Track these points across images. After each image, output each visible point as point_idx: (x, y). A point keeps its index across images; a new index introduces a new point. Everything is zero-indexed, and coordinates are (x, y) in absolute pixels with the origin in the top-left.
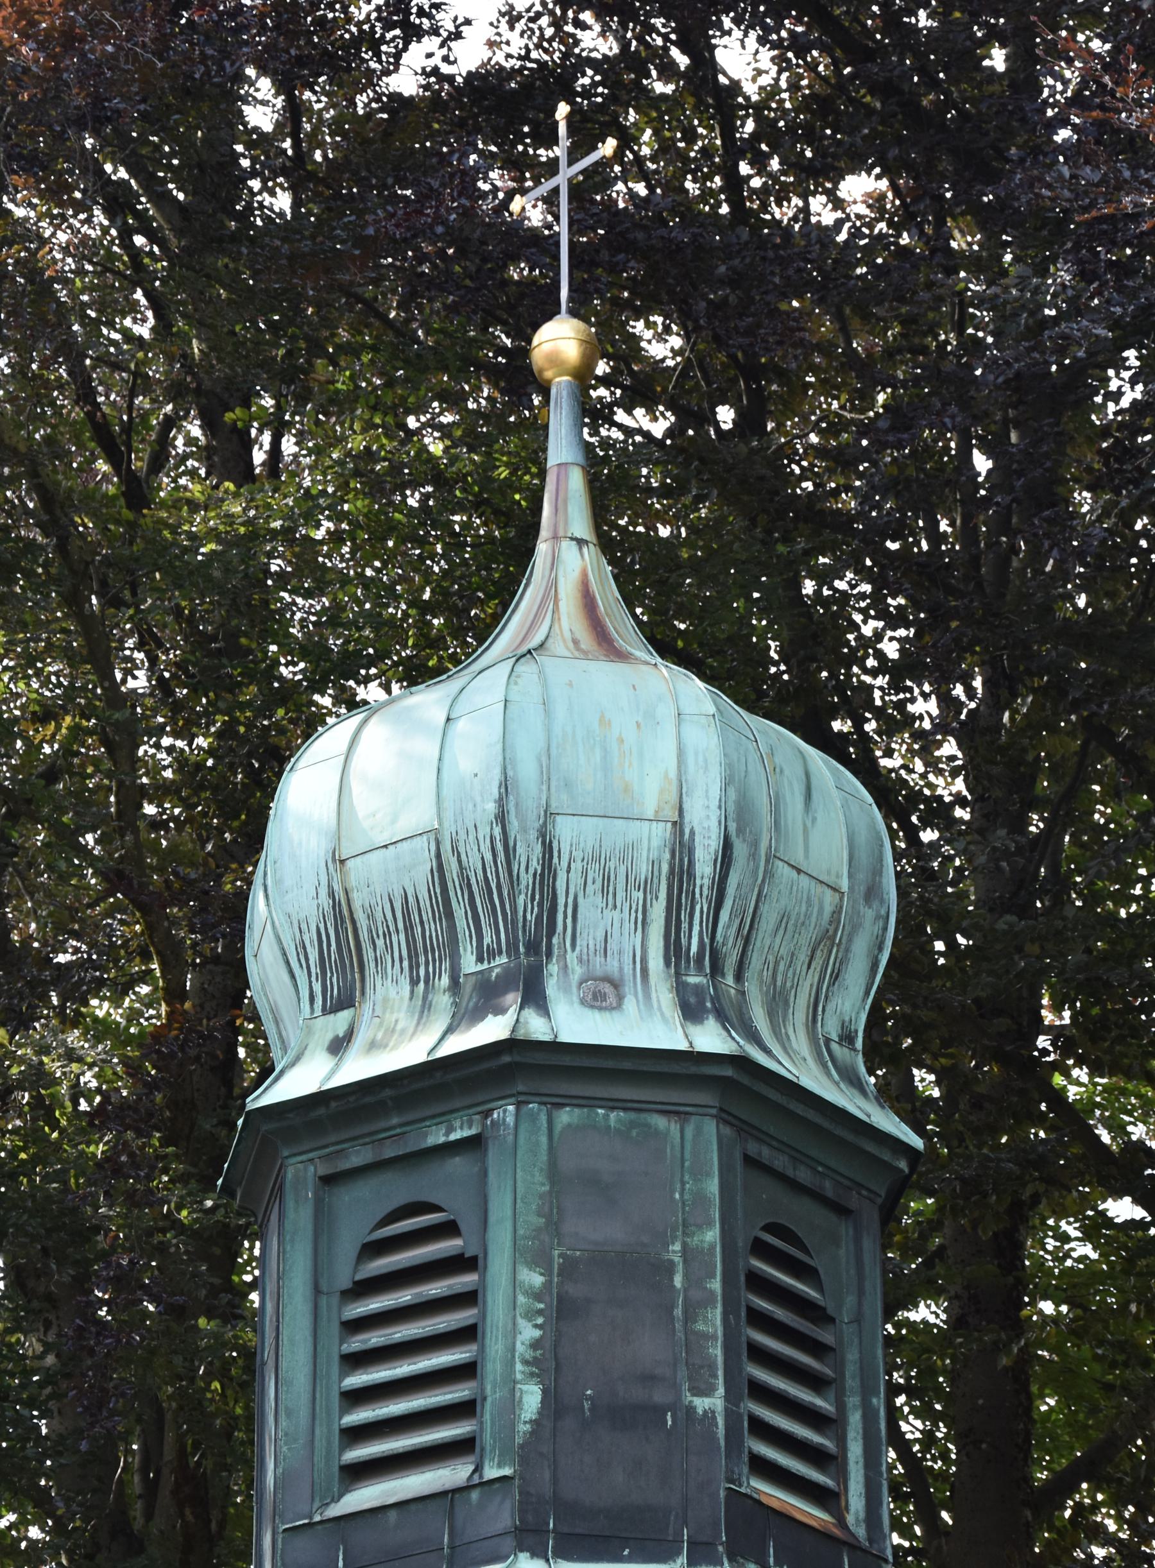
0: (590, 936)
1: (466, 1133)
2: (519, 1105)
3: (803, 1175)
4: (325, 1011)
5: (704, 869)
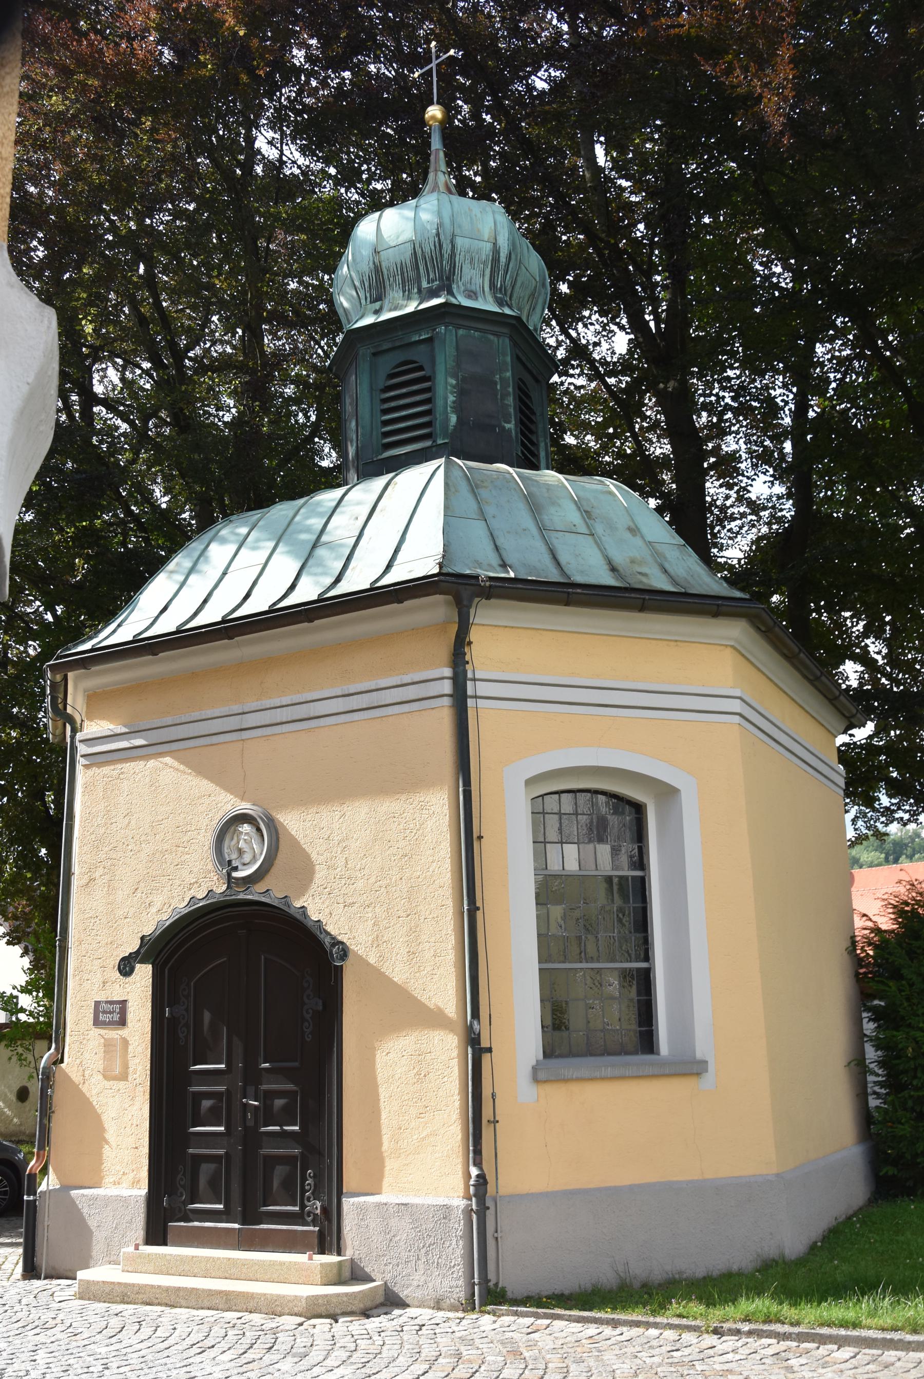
0: (466, 278)
1: (427, 336)
2: (446, 327)
3: (529, 365)
4: (371, 302)
5: (503, 260)
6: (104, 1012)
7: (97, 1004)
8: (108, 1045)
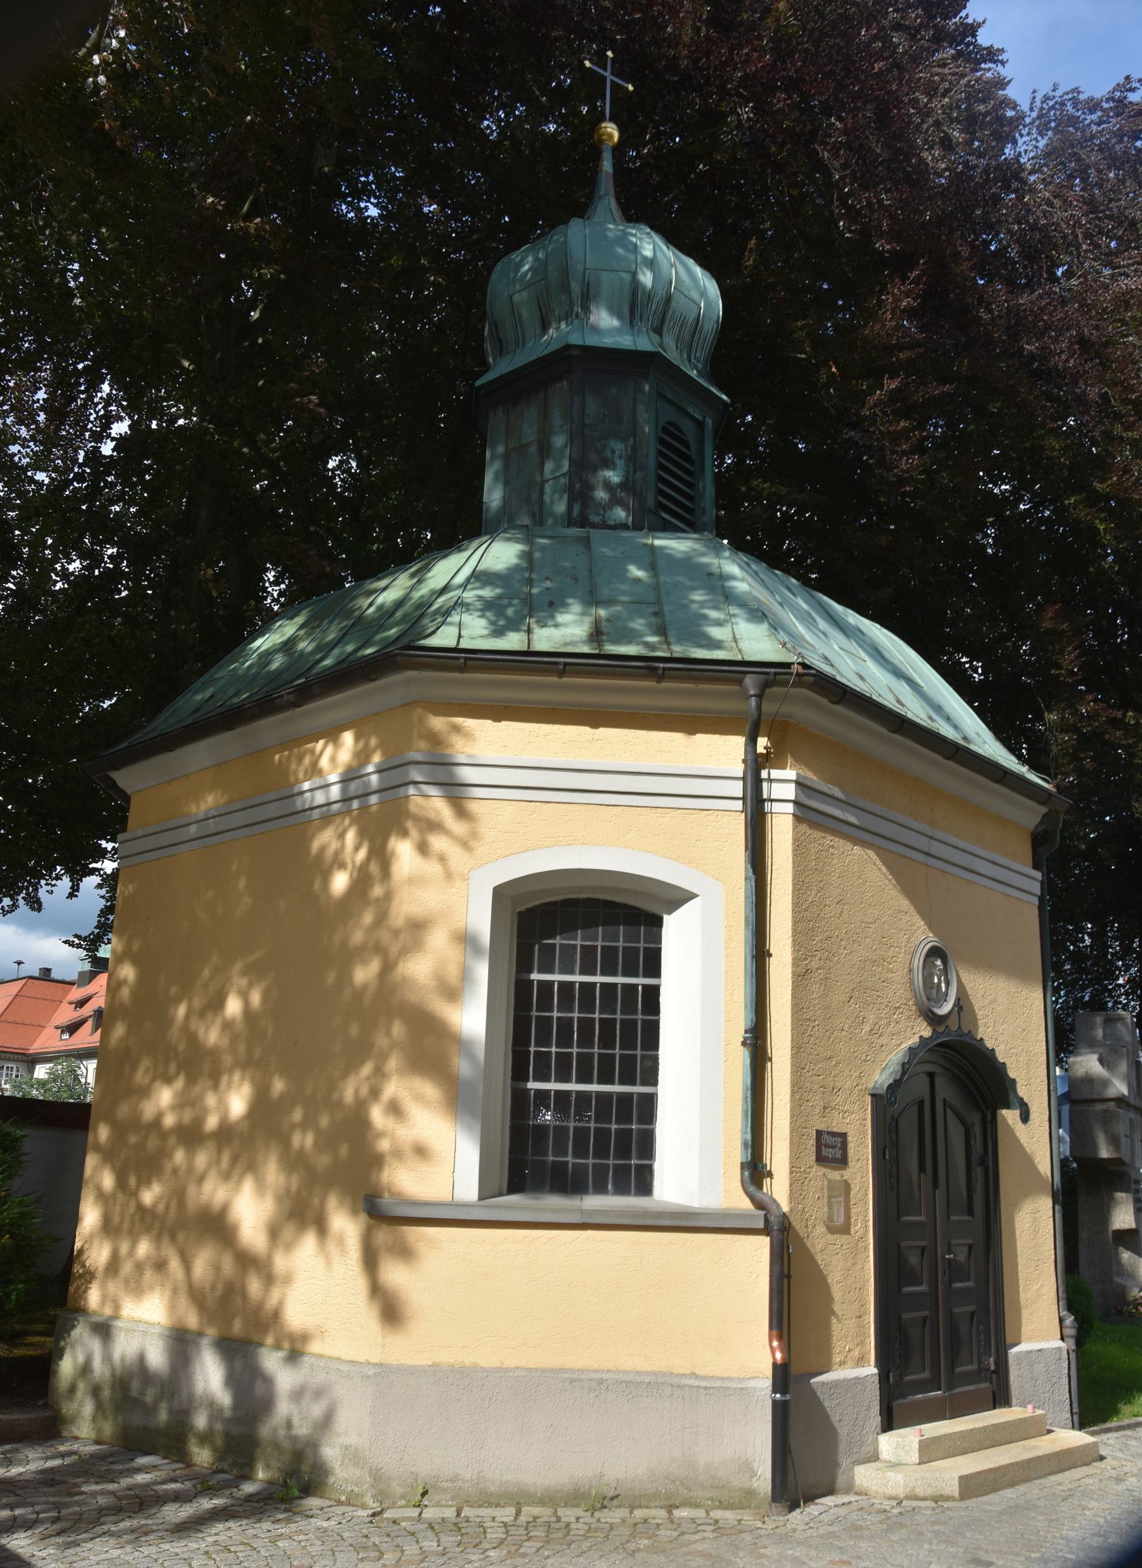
6: (827, 1146)
7: (819, 1133)
8: (831, 1185)
